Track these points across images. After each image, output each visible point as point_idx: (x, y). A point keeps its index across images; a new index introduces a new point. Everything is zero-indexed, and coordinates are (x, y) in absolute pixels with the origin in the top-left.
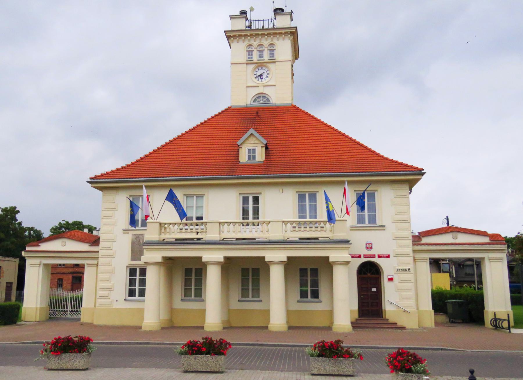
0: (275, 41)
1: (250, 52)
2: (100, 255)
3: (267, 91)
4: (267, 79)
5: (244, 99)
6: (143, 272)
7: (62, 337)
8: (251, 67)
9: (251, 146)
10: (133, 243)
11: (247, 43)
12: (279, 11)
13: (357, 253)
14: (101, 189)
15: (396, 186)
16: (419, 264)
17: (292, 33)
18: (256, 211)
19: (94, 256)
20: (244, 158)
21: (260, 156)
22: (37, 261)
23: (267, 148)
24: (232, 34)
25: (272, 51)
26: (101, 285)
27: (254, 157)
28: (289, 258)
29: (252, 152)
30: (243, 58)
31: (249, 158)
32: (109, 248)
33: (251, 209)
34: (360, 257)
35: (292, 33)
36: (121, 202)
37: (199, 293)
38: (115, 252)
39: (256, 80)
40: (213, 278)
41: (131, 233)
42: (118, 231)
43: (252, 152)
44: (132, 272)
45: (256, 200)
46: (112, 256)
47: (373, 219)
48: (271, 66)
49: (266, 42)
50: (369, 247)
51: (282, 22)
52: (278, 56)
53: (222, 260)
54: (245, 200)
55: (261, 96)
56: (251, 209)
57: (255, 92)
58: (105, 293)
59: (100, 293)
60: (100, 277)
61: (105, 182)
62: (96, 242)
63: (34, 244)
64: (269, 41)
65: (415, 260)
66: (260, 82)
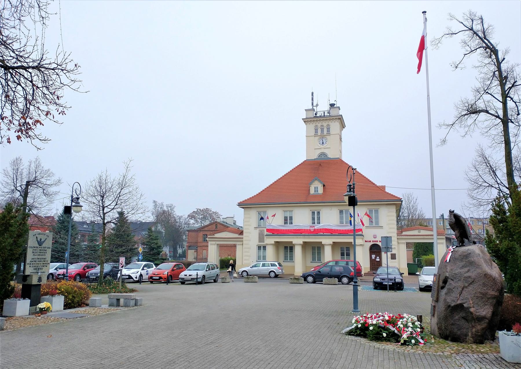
0: (330, 123)
1: (316, 131)
2: (244, 239)
3: (326, 151)
4: (326, 145)
5: (314, 156)
6: (264, 248)
7: (387, 190)
8: (317, 138)
9: (316, 186)
10: (259, 234)
11: (314, 125)
12: (332, 105)
13: (369, 240)
14: (243, 208)
15: (388, 206)
16: (400, 245)
17: (339, 119)
18: (319, 219)
19: (241, 240)
20: (312, 191)
21: (321, 191)
22: (214, 243)
23: (324, 186)
24: (306, 120)
27: (317, 191)
28: (334, 242)
29: (316, 189)
30: (313, 133)
31: (315, 191)
33: (316, 217)
34: (370, 242)
35: (339, 119)
36: (254, 215)
37: (292, 258)
38: (251, 238)
39: (320, 145)
40: (298, 251)
41: (258, 229)
43: (316, 189)
44: (259, 248)
45: (319, 213)
46: (250, 240)
47: (377, 223)
48: (328, 137)
49: (325, 124)
50: (375, 237)
51: (334, 112)
52: (332, 131)
53: (273, 243)
54: (313, 213)
55: (323, 154)
56: (316, 217)
57: (319, 152)
59: (244, 258)
61: (244, 205)
62: (241, 233)
64: (327, 123)
65: (398, 243)
66: (322, 146)
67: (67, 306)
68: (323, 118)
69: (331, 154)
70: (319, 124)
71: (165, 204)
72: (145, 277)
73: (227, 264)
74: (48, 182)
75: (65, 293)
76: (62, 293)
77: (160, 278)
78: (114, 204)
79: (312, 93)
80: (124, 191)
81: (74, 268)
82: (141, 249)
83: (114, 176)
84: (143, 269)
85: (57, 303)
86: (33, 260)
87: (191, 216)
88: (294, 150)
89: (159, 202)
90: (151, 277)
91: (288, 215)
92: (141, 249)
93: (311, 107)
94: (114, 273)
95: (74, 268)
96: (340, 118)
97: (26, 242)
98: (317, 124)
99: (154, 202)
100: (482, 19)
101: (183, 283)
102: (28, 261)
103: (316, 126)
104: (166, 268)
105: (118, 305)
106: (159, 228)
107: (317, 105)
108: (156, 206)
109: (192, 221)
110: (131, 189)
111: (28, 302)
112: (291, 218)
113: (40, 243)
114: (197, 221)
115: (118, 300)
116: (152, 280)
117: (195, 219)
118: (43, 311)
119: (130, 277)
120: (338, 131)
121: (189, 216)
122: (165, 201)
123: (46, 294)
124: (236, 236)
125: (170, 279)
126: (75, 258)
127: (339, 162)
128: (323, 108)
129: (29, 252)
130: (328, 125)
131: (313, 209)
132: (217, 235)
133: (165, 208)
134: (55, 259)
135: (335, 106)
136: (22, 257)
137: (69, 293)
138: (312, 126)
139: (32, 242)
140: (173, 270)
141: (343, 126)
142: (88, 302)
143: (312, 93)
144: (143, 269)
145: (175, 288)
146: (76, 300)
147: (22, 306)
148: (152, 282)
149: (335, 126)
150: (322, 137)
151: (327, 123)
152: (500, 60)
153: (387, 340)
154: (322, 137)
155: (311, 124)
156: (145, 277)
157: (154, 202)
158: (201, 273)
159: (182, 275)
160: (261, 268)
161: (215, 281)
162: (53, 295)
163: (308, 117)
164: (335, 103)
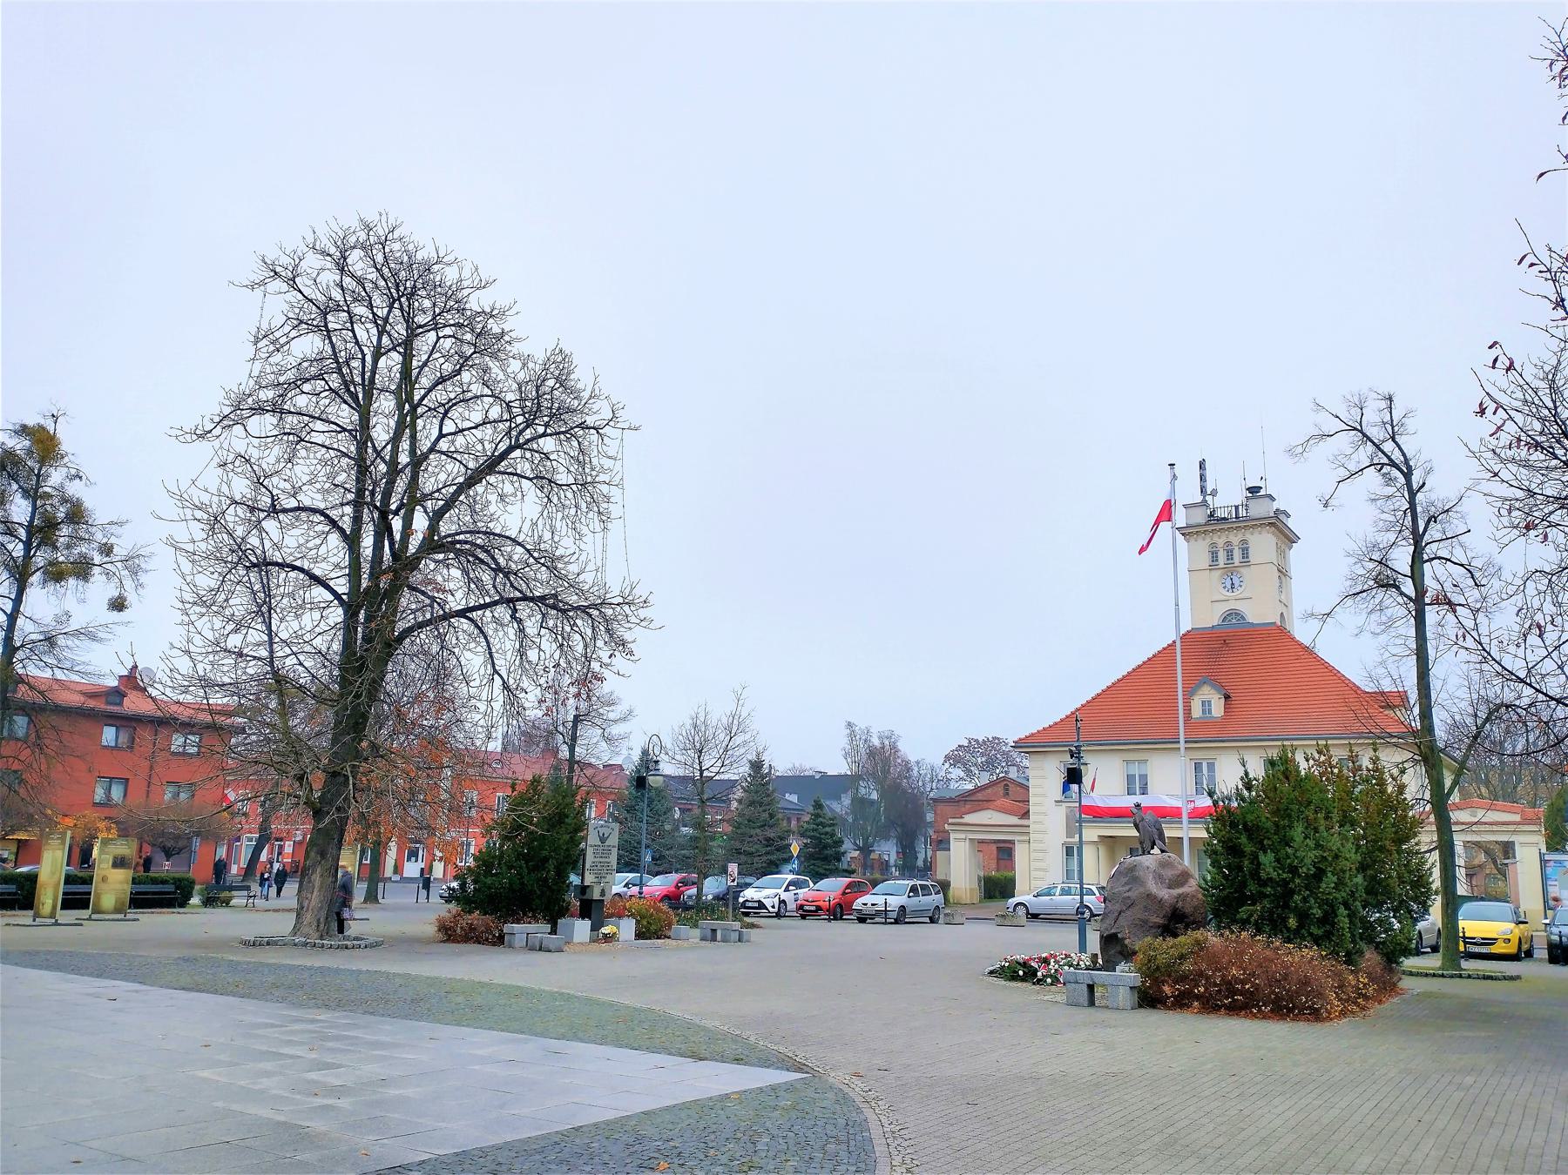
0: (1248, 536)
3: (1240, 606)
5: (1211, 618)
9: (1205, 698)
11: (1208, 540)
12: (1254, 490)
19: (1024, 830)
20: (1197, 712)
21: (1218, 709)
23: (1227, 697)
25: (1245, 553)
26: (1034, 865)
29: (1206, 704)
30: (1205, 561)
32: (1040, 786)
42: (1049, 803)
43: (1206, 704)
44: (1069, 851)
45: (1211, 767)
46: (1044, 832)
49: (1235, 539)
51: (1259, 509)
54: (1198, 767)
57: (1223, 608)
58: (1040, 855)
60: (1033, 855)
63: (174, 708)
64: (1240, 537)
67: (640, 935)
68: (1236, 522)
69: (1258, 612)
70: (1221, 540)
71: (874, 731)
72: (792, 906)
73: (997, 888)
74: (612, 716)
75: (640, 917)
76: (632, 915)
77: (819, 908)
78: (719, 764)
79: (1202, 465)
80: (738, 740)
81: (658, 885)
82: (795, 849)
83: (719, 713)
84: (787, 890)
85: (627, 928)
86: (594, 865)
87: (954, 759)
88: (1147, 606)
89: (861, 724)
90: (801, 907)
91: (1136, 770)
92: (795, 849)
93: (1199, 499)
94: (728, 899)
95: (658, 885)
96: (1277, 524)
97: (585, 838)
98: (1216, 539)
99: (850, 725)
100: (1391, 399)
101: (862, 920)
102: (587, 866)
103: (1213, 545)
104: (831, 888)
105: (714, 939)
106: (862, 791)
107: (1214, 493)
108: (852, 735)
109: (957, 772)
110: (747, 736)
111: (587, 923)
112: (1144, 778)
113: (603, 839)
114: (968, 772)
115: (714, 931)
116: (804, 913)
117: (965, 765)
118: (608, 938)
119: (761, 905)
120: (1272, 556)
121: (947, 758)
122: (877, 725)
123: (611, 916)
124: (1014, 820)
125: (838, 911)
126: (660, 866)
127: (1278, 634)
128: (1229, 497)
129: (589, 852)
130: (1244, 542)
131: (1199, 755)
132: (969, 819)
133: (876, 742)
134: (627, 864)
135: (1262, 492)
136: (574, 860)
137: (639, 913)
138: (1202, 545)
139: (593, 839)
140: (844, 893)
141: (1290, 538)
142: (671, 933)
143: (1202, 465)
144: (787, 890)
145: (847, 931)
146: (653, 928)
147: (582, 928)
148: (803, 917)
149: (1263, 544)
150: (1230, 571)
151: (1240, 537)
152: (1415, 486)
153: (1023, 979)
154: (1230, 571)
155: (1200, 541)
156: (792, 906)
157: (850, 725)
158: (895, 902)
159: (858, 904)
160: (1057, 898)
161: (932, 920)
162: (620, 917)
163: (1192, 522)
164: (1261, 484)
